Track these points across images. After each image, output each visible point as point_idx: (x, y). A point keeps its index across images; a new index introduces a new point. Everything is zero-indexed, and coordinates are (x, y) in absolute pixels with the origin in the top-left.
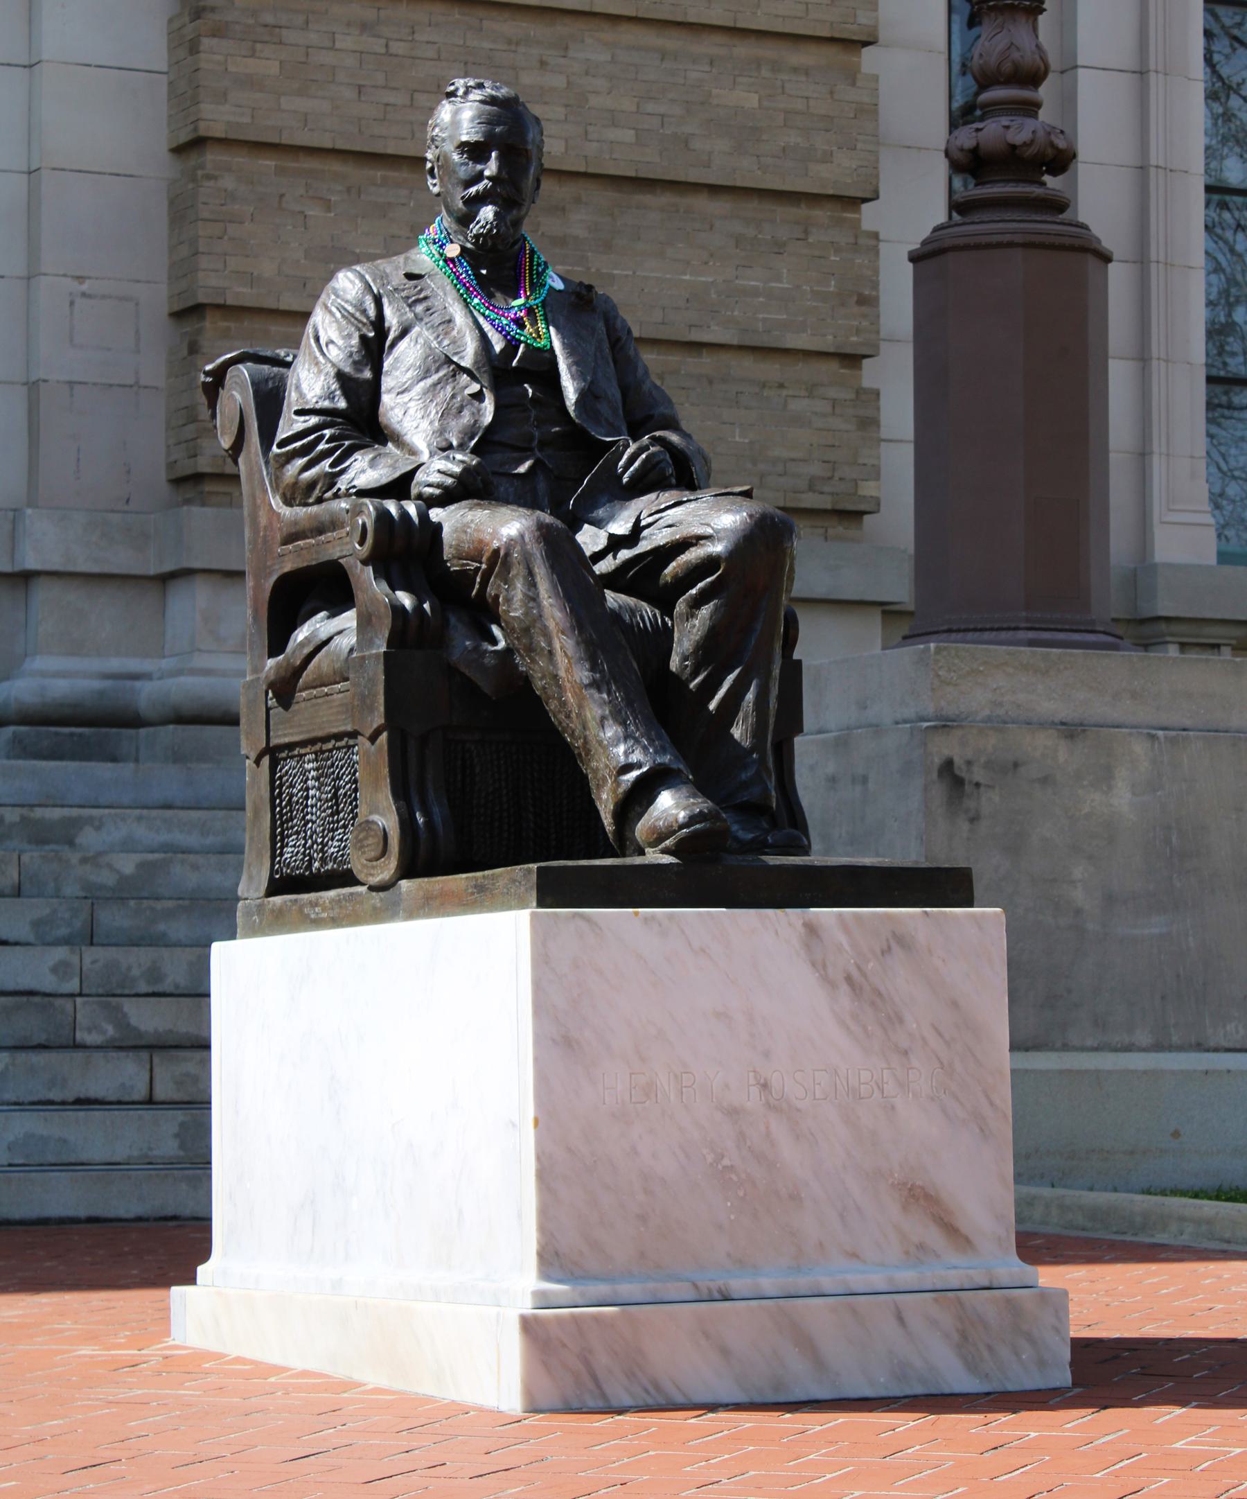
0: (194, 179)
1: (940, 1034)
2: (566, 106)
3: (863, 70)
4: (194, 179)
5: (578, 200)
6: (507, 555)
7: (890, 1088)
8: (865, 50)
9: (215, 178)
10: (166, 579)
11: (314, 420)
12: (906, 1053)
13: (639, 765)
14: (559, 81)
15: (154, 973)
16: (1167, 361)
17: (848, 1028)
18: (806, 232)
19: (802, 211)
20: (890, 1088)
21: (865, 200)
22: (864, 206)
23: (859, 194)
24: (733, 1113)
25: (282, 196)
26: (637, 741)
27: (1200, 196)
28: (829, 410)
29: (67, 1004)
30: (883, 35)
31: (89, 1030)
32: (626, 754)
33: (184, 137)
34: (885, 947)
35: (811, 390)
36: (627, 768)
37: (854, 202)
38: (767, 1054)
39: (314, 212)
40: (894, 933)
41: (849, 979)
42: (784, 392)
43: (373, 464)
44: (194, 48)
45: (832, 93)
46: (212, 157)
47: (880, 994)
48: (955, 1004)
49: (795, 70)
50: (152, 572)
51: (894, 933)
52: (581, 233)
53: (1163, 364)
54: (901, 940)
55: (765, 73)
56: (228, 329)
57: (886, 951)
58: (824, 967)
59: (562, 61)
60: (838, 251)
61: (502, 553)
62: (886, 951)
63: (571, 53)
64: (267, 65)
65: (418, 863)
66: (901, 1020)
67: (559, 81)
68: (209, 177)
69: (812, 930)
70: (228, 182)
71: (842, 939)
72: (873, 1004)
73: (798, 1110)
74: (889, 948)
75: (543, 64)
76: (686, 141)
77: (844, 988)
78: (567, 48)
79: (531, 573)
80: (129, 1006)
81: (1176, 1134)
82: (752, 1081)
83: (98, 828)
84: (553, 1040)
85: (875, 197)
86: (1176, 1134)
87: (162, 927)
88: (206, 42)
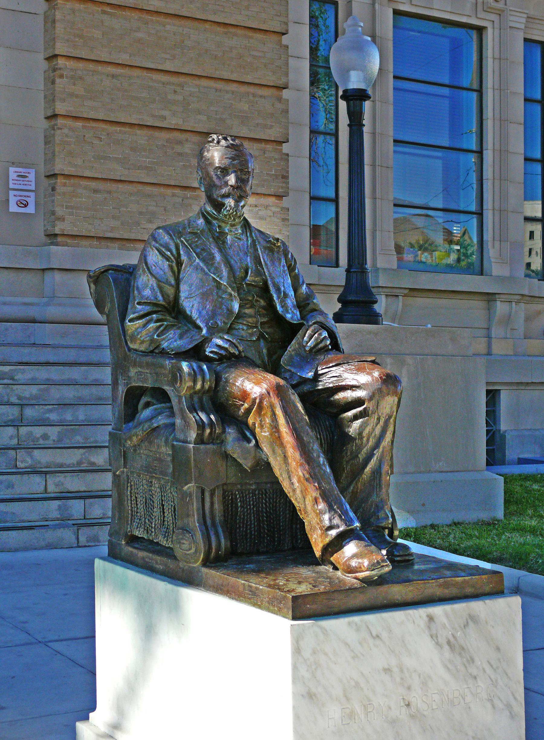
0: (54, 129)
1: (492, 666)
2: (183, 107)
3: (283, 98)
4: (54, 129)
5: (187, 140)
6: (261, 402)
7: (469, 698)
8: (284, 90)
9: (61, 129)
10: (43, 270)
11: (148, 309)
12: (475, 678)
13: (338, 527)
14: (180, 98)
15: (45, 437)
16: (381, 199)
17: (448, 669)
18: (264, 153)
19: (263, 145)
20: (469, 698)
21: (284, 142)
22: (284, 144)
23: (282, 140)
24: (393, 722)
25: (84, 136)
26: (336, 512)
27: (392, 142)
28: (272, 215)
29: (12, 452)
30: (290, 85)
31: (22, 462)
32: (330, 520)
33: (49, 114)
34: (466, 623)
35: (267, 207)
36: (331, 528)
37: (281, 143)
38: (409, 688)
39: (96, 142)
40: (469, 615)
41: (449, 643)
42: (257, 209)
43: (181, 337)
44: (53, 82)
45: (273, 105)
46: (60, 121)
47: (463, 649)
48: (498, 649)
49: (261, 97)
50: (39, 268)
51: (469, 615)
52: (187, 151)
53: (380, 200)
54: (473, 618)
55: (251, 97)
56: (66, 183)
57: (466, 625)
58: (437, 637)
59: (182, 91)
60: (275, 159)
61: (257, 401)
62: (466, 625)
63: (185, 88)
64: (79, 89)
65: (213, 561)
66: (473, 660)
67: (180, 98)
68: (59, 129)
69: (431, 618)
70: (66, 131)
71: (445, 620)
72: (460, 654)
73: (425, 716)
74: (467, 623)
75: (175, 92)
76: (223, 120)
77: (446, 647)
78: (183, 87)
79: (274, 414)
80: (36, 452)
81: (423, 505)
82: (402, 704)
83: (23, 373)
84: (302, 695)
85: (287, 141)
86: (423, 505)
87: (47, 415)
88: (58, 80)
